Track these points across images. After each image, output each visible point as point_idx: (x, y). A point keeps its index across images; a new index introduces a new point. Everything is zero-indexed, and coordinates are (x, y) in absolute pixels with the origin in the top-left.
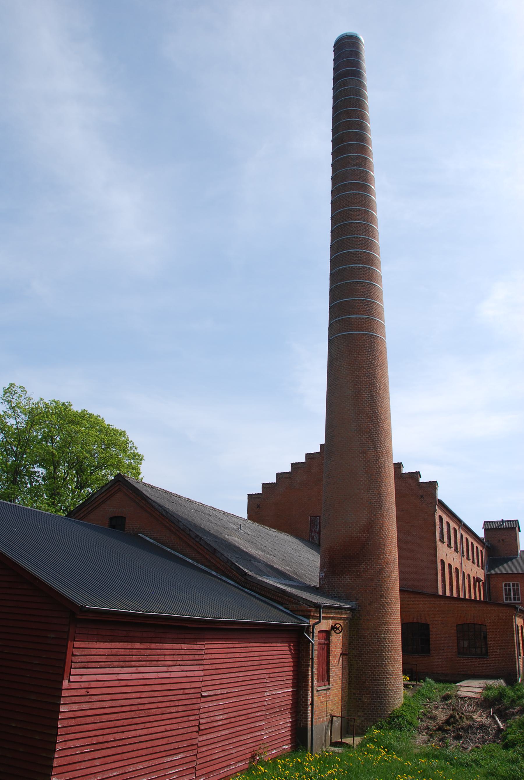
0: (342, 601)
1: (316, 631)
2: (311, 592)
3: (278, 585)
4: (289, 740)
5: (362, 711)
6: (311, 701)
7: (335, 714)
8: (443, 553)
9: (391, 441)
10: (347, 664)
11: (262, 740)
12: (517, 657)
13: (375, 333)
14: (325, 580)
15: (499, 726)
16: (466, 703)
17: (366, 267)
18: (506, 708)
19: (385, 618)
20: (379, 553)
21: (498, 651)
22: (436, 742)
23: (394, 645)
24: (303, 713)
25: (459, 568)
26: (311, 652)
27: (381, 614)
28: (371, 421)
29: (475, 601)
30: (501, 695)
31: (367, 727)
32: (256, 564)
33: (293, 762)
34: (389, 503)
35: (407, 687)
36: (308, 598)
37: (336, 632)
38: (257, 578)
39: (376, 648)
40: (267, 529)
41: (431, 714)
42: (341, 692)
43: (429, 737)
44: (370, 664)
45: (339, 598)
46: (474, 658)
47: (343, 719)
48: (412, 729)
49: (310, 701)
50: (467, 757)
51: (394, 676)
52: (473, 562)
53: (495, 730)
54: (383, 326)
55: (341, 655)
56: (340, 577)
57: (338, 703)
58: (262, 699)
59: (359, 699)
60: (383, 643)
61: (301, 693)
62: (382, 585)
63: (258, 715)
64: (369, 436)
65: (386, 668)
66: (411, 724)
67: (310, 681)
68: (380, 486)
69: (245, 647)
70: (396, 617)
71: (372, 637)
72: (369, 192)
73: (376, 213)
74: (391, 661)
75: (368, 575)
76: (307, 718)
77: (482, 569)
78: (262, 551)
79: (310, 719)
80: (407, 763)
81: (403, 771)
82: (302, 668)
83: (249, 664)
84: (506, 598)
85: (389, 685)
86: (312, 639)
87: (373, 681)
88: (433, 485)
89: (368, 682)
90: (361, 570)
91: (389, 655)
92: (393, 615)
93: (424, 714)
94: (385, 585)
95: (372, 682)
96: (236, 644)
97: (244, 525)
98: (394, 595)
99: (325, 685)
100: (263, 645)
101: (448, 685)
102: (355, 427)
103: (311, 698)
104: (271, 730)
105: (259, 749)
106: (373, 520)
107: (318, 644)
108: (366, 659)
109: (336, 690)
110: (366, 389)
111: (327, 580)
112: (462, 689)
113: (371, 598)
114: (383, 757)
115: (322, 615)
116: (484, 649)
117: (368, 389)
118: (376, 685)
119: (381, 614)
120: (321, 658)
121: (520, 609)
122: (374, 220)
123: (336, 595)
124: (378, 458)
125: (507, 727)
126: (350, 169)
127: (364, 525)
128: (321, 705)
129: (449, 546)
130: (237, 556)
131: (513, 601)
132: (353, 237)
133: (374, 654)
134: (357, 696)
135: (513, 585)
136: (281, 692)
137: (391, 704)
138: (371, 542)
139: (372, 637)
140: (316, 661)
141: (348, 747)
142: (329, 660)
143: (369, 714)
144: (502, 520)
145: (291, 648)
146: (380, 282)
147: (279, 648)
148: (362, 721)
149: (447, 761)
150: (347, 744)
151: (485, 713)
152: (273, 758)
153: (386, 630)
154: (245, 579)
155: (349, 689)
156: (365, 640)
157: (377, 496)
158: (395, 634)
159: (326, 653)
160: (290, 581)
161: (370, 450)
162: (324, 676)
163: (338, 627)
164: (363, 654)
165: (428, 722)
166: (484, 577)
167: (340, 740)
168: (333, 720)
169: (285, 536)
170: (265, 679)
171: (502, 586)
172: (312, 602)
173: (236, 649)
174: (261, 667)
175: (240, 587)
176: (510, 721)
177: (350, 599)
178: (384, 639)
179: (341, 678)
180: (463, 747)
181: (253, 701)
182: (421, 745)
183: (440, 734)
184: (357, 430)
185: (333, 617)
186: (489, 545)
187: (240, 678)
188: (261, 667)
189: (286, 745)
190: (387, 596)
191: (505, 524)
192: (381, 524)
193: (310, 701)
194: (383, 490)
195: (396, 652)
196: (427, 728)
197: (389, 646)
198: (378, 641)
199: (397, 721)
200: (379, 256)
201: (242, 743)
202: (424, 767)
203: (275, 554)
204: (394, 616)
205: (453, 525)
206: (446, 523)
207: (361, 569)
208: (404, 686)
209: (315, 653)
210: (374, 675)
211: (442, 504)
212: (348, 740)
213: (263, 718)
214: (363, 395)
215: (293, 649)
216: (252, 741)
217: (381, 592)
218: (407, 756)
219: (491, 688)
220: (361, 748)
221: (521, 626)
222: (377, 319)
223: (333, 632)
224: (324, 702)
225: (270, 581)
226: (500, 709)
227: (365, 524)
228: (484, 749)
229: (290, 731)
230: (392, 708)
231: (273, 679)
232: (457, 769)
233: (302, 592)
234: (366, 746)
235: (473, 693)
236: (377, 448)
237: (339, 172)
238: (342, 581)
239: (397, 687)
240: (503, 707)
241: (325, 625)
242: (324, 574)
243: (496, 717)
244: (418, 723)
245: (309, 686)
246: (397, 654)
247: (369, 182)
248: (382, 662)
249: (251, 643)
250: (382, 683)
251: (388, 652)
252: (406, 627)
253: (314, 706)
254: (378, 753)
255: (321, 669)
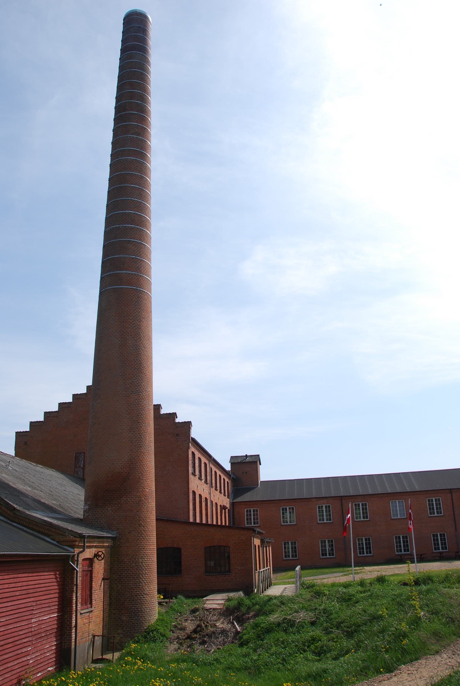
0: (104, 530)
1: (80, 559)
2: (76, 524)
3: (46, 519)
4: (54, 662)
5: (121, 629)
6: (74, 623)
7: (96, 633)
8: (195, 485)
9: (152, 387)
10: (108, 588)
11: (28, 664)
12: (254, 572)
13: (143, 289)
14: (89, 512)
15: (237, 630)
16: (211, 613)
17: (138, 228)
18: (244, 614)
19: (142, 545)
20: (138, 486)
21: (239, 568)
22: (185, 649)
23: (150, 568)
24: (67, 635)
25: (208, 498)
26: (75, 578)
27: (139, 541)
28: (135, 368)
29: (221, 526)
30: (240, 604)
31: (125, 642)
32: (24, 499)
33: (57, 682)
34: (148, 442)
35: (161, 605)
36: (73, 529)
37: (99, 559)
38: (25, 513)
39: (134, 571)
40: (34, 465)
41: (181, 625)
42: (102, 613)
43: (179, 645)
44: (129, 586)
45: (102, 529)
46: (219, 575)
47: (104, 637)
48: (165, 640)
49: (74, 624)
50: (210, 658)
51: (150, 596)
52: (220, 492)
53: (233, 633)
54: (149, 283)
55: (102, 580)
56: (103, 509)
57: (100, 623)
58: (30, 626)
59: (119, 618)
60: (141, 567)
61: (66, 617)
62: (140, 515)
63: (25, 641)
64: (132, 381)
65: (143, 589)
66: (164, 636)
67: (74, 605)
68: (141, 426)
69: (14, 578)
70: (153, 543)
71: (131, 562)
72: (145, 160)
73: (150, 179)
74: (147, 583)
75: (128, 507)
76: (71, 640)
77: (228, 498)
78: (30, 487)
79: (73, 641)
80: (161, 669)
81: (157, 675)
82: (67, 594)
83: (17, 593)
84: (247, 523)
85: (146, 604)
86: (77, 567)
87: (131, 601)
88: (187, 425)
89: (127, 603)
90: (122, 502)
91: (146, 577)
92: (149, 541)
93: (175, 626)
94: (143, 515)
95: (130, 602)
96: (5, 576)
97: (12, 462)
98: (151, 523)
99: (87, 608)
100: (31, 575)
101: (196, 600)
102: (121, 373)
103: (75, 621)
104: (37, 654)
105: (26, 674)
106: (133, 457)
107: (82, 571)
108: (125, 582)
109: (98, 612)
110: (131, 339)
111: (90, 512)
112: (208, 602)
113: (130, 527)
114: (139, 666)
115: (86, 544)
116: (227, 567)
117: (134, 339)
118: (134, 604)
119: (139, 541)
120: (84, 584)
121: (258, 532)
122: (148, 186)
123: (98, 526)
124: (140, 401)
125: (243, 629)
126: (129, 137)
127: (125, 461)
128: (84, 626)
129: (200, 478)
130: (6, 492)
131: (253, 525)
132: (128, 200)
133: (133, 577)
134: (117, 616)
135: (254, 511)
136: (47, 618)
137: (147, 620)
138: (132, 477)
139: (131, 562)
140: (80, 586)
141: (108, 662)
142: (92, 585)
143: (128, 631)
144: (246, 455)
145: (56, 576)
146: (149, 242)
147: (46, 577)
148: (121, 638)
149: (194, 663)
150: (107, 659)
151: (226, 620)
152: (39, 681)
153: (143, 555)
154: (14, 514)
155: (109, 610)
156: (125, 565)
157: (138, 435)
158: (151, 558)
159: (89, 580)
160: (57, 514)
161: (133, 394)
162: (87, 600)
163: (100, 554)
164: (122, 578)
165: (179, 633)
166: (229, 505)
167: (101, 657)
168: (95, 639)
169: (52, 472)
170: (32, 607)
171: (244, 512)
172: (77, 533)
173: (5, 580)
174: (29, 596)
175: (9, 521)
176: (246, 625)
177: (111, 529)
178: (141, 563)
179: (103, 600)
180: (207, 650)
181: (20, 628)
182: (172, 653)
183: (189, 642)
184: (121, 376)
185: (96, 546)
186: (235, 477)
187: (8, 607)
188: (29, 596)
189: (51, 666)
190: (145, 525)
191: (248, 458)
192: (141, 460)
193: (74, 624)
194: (144, 431)
195: (152, 574)
196: (178, 638)
197: (145, 569)
198: (136, 565)
199: (152, 635)
200: (150, 219)
201: (9, 669)
202: (174, 670)
203: (42, 489)
204: (151, 543)
205: (204, 460)
206: (198, 458)
207: (122, 501)
208: (158, 604)
209: (79, 579)
210: (132, 596)
211: (195, 442)
212: (109, 656)
213: (29, 643)
214: (129, 344)
215: (58, 577)
216: (19, 667)
217: (139, 521)
218: (160, 664)
219: (232, 599)
220: (120, 661)
221: (259, 546)
222: (145, 276)
223: (95, 559)
224: (87, 623)
225: (38, 515)
226: (238, 616)
227: (126, 460)
228: (223, 650)
229: (54, 654)
230: (147, 624)
231: (40, 606)
232: (201, 668)
233: (68, 524)
234: (124, 659)
235: (217, 605)
236: (139, 393)
237: (119, 138)
238: (104, 513)
239: (152, 605)
240: (241, 614)
241: (89, 553)
242: (88, 507)
243: (235, 622)
244: (170, 635)
245: (73, 610)
246: (153, 576)
247: (146, 151)
248: (139, 583)
249: (20, 574)
250: (139, 602)
251: (144, 575)
252: (160, 551)
253: (78, 628)
254: (135, 663)
255: (85, 594)
